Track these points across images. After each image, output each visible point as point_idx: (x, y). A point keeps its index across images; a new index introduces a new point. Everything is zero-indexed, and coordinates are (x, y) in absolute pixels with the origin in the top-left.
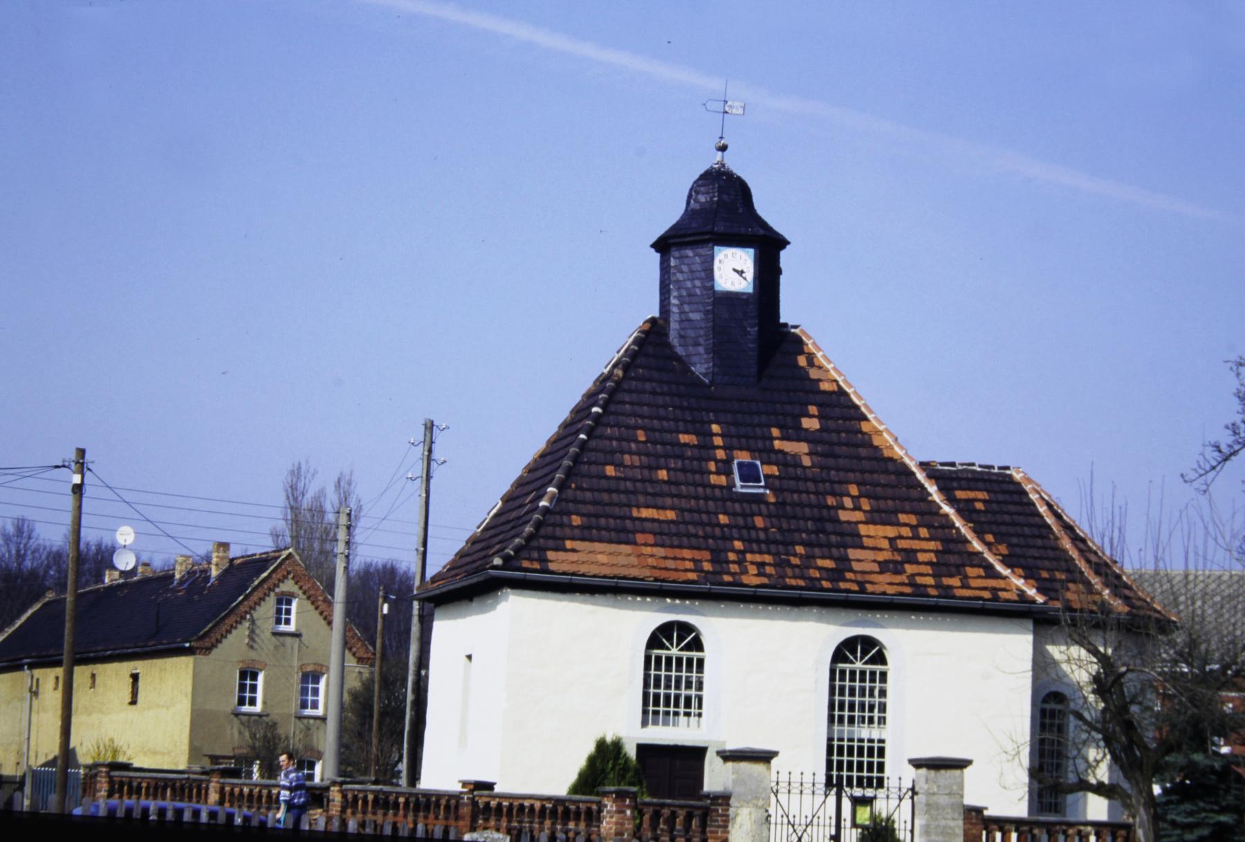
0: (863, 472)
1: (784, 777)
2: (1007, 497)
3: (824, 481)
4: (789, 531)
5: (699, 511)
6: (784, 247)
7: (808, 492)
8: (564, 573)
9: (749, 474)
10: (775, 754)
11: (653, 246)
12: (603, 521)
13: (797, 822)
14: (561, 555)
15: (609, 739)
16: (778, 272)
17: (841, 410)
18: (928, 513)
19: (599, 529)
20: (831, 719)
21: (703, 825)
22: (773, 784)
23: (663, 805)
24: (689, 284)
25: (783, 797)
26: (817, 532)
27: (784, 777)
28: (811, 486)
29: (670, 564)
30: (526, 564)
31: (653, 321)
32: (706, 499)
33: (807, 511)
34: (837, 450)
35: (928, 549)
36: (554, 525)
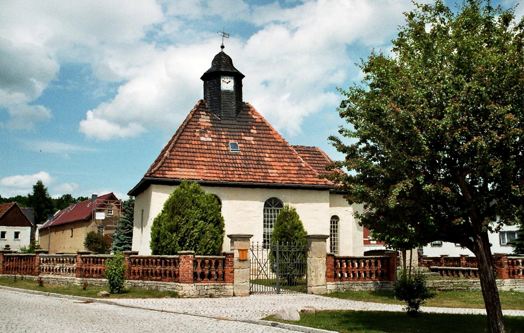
0: (271, 146)
1: (255, 244)
2: (315, 156)
3: (259, 149)
4: (248, 164)
5: (218, 158)
6: (242, 78)
7: (254, 152)
8: (171, 178)
9: (235, 146)
10: (252, 236)
11: (201, 78)
12: (185, 162)
13: (261, 262)
14: (171, 173)
15: (36, 184)
16: (241, 86)
17: (263, 126)
18: (293, 160)
19: (184, 164)
20: (265, 226)
21: (224, 266)
22: (251, 247)
23: (206, 259)
24: (213, 88)
25: (255, 253)
26: (257, 164)
27: (255, 244)
28: (255, 151)
29: (209, 175)
30: (158, 175)
31: (202, 101)
32: (220, 154)
33: (254, 158)
34: (263, 139)
35: (294, 169)
36: (168, 163)
